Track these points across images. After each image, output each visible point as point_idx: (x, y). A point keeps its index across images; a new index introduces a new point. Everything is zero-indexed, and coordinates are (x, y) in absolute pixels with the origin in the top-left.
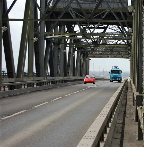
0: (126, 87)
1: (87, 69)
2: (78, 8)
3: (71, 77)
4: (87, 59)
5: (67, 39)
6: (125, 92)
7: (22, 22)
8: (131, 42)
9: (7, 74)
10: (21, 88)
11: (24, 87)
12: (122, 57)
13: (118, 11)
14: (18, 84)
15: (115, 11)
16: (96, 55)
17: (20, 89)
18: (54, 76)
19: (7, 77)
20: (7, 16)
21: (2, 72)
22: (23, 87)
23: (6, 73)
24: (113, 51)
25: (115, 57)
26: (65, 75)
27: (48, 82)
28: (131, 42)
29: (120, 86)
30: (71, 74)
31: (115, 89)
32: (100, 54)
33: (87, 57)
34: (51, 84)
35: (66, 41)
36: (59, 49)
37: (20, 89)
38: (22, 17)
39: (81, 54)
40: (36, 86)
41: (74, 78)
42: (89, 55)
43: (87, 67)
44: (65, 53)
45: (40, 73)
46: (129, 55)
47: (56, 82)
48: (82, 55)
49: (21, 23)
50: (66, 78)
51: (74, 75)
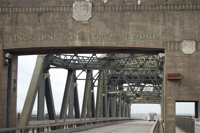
0: (158, 124)
1: (129, 112)
2: (128, 75)
3: (121, 118)
4: (129, 105)
5: (94, 81)
6: (158, 131)
7: (97, 87)
8: (161, 96)
9: (36, 116)
10: (63, 128)
11: (66, 128)
12: (155, 103)
13: (152, 76)
14: (60, 125)
15: (151, 76)
16: (136, 102)
17: (62, 129)
18: (111, 117)
19: (48, 118)
20: (94, 85)
21: (46, 115)
22: (65, 127)
23: (45, 115)
24: (149, 100)
25: (150, 103)
26: (117, 116)
27: (75, 124)
28: (161, 96)
29: (155, 123)
30: (120, 116)
31: (152, 125)
32: (139, 101)
33: (129, 103)
34: (67, 127)
35: (94, 82)
36: (114, 99)
37: (62, 129)
38: (85, 78)
39: (125, 101)
40: (77, 126)
41: (110, 118)
42: (131, 102)
43: (129, 110)
44: (93, 93)
45: (105, 115)
46: (160, 102)
47: (57, 128)
48: (126, 102)
49: (85, 81)
50: (117, 118)
51: (122, 117)
